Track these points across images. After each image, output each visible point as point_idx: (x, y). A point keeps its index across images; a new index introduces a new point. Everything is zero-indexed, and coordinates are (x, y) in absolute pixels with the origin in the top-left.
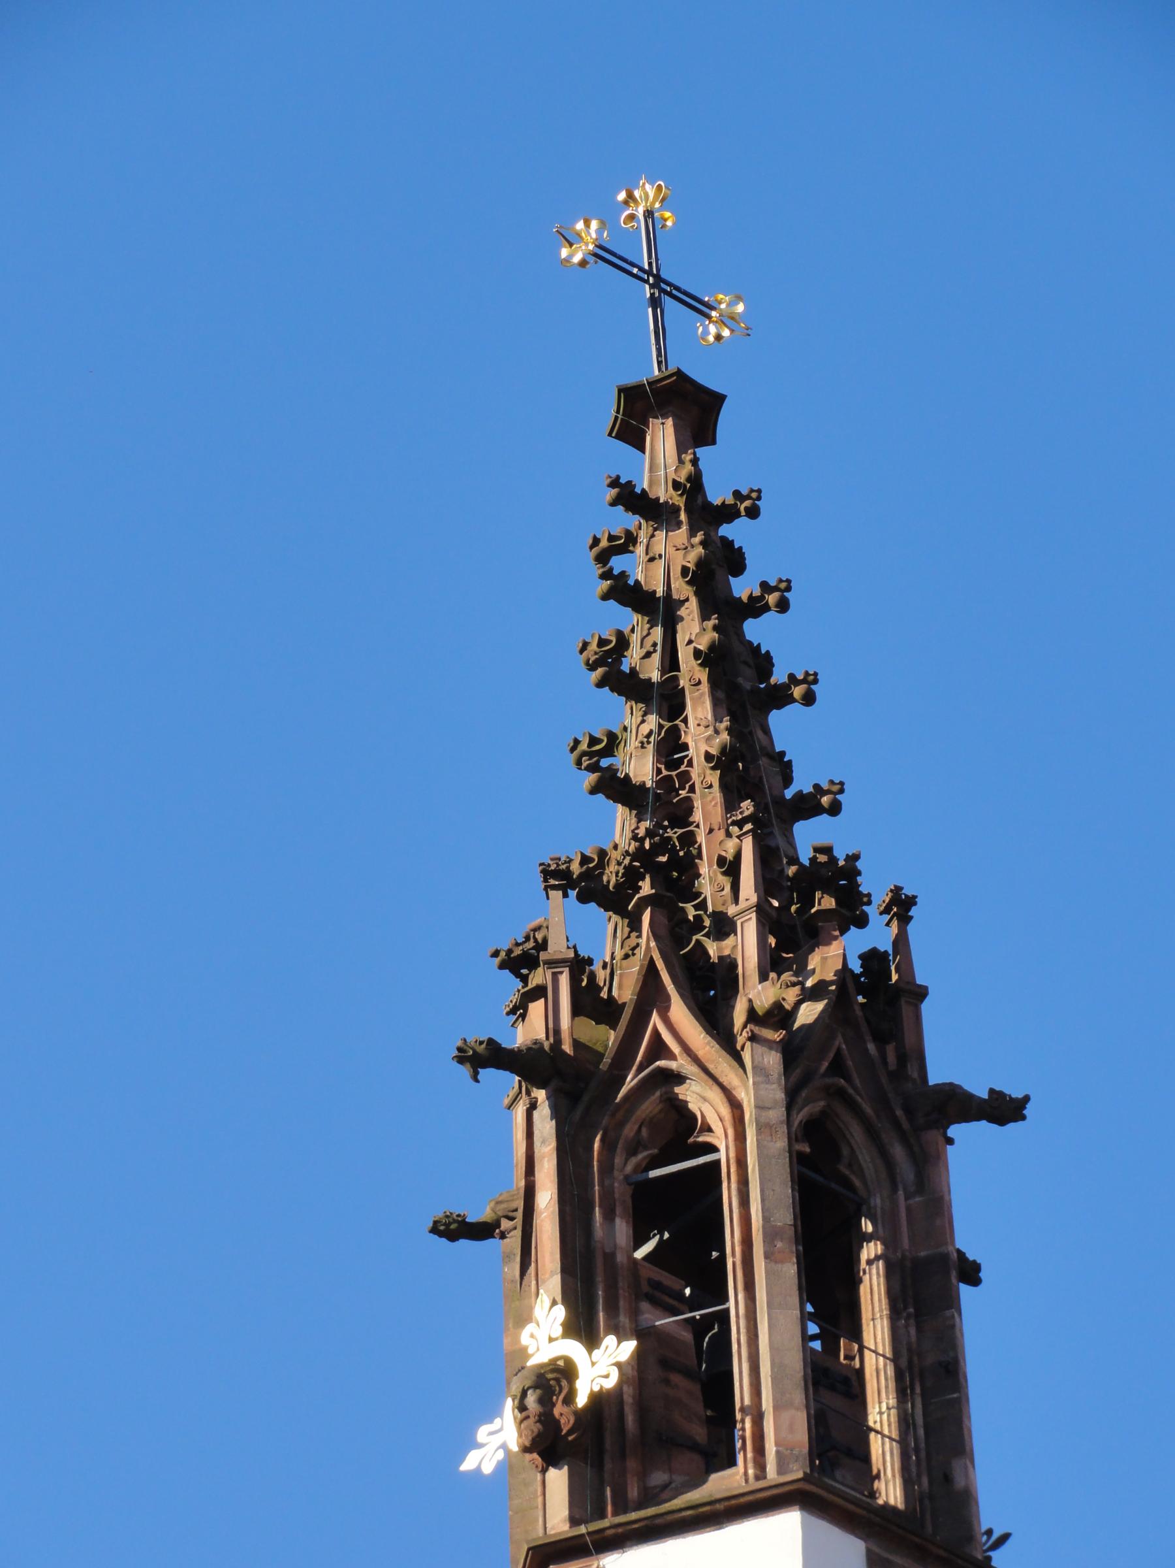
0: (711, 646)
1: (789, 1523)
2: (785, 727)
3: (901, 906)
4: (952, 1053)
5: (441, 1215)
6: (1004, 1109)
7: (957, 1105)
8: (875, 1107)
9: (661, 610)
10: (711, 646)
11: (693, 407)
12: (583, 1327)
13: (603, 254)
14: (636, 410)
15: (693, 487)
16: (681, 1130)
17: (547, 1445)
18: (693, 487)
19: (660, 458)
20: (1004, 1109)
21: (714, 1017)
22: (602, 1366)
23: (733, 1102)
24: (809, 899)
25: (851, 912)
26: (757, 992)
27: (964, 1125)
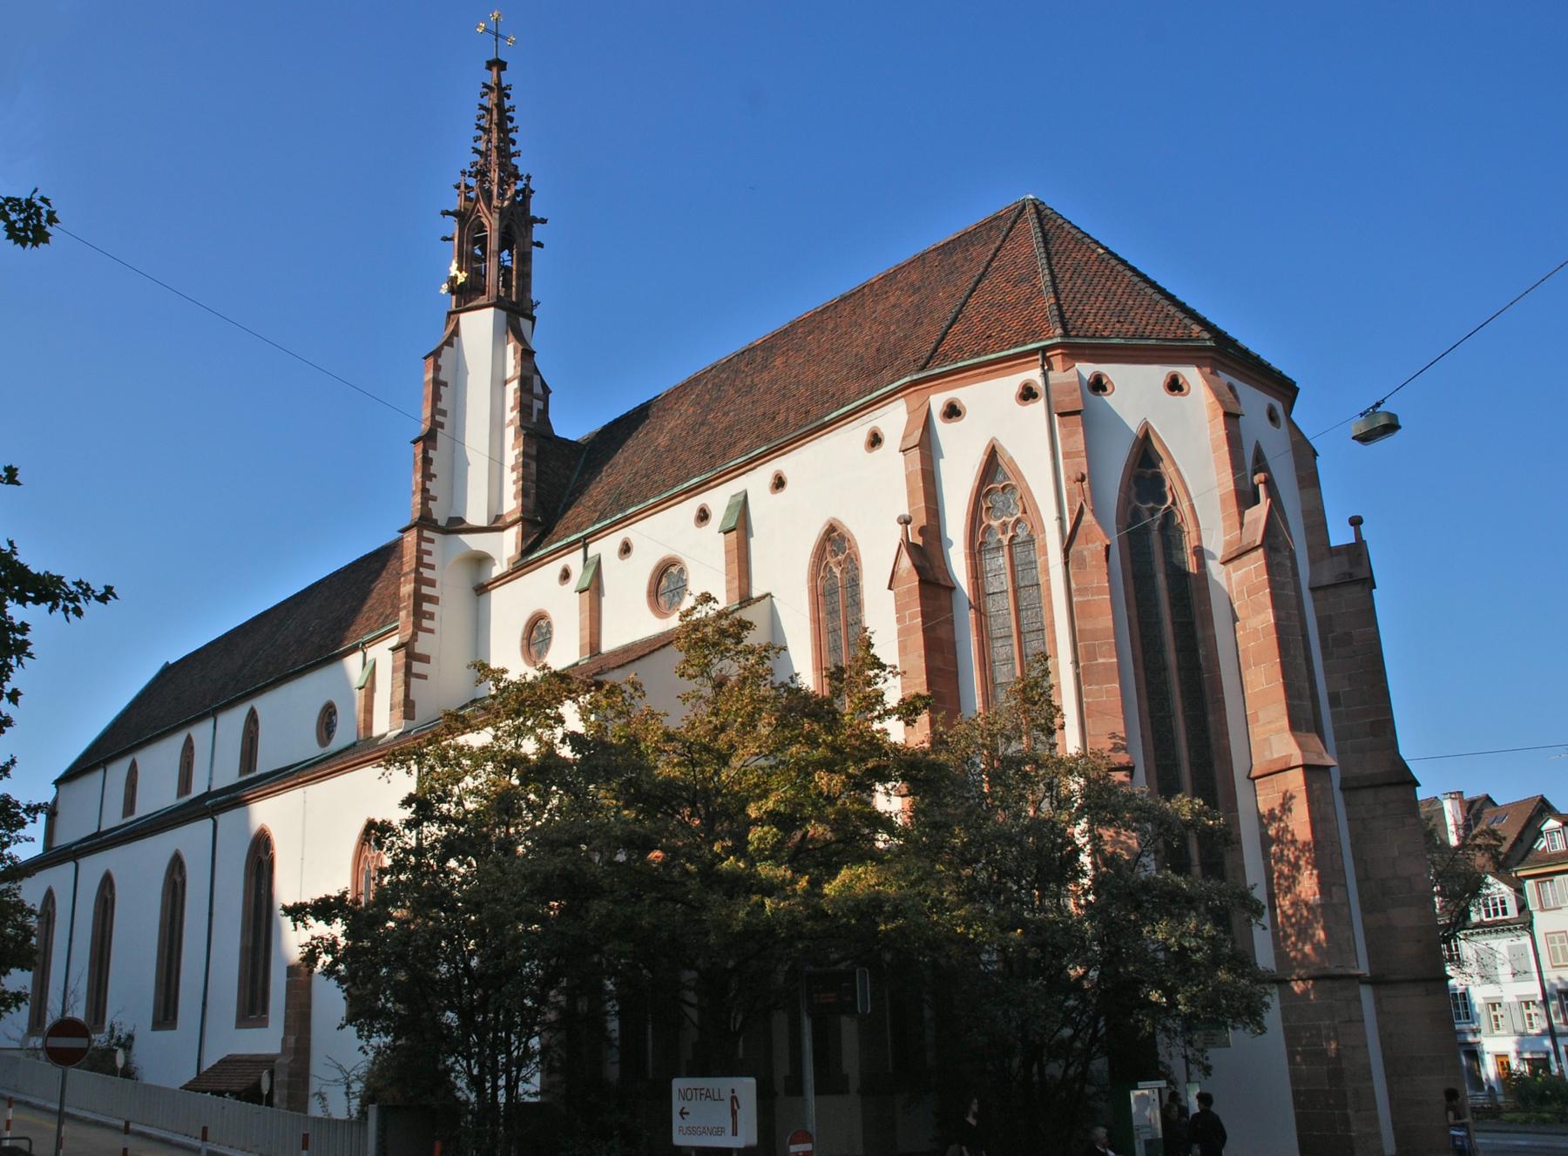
0: (500, 120)
1: (492, 310)
2: (431, 504)
3: (529, 178)
4: (534, 211)
5: (378, 820)
6: (544, 221)
7: (535, 220)
8: (518, 225)
9: (487, 131)
10: (500, 120)
11: (500, 65)
12: (460, 269)
13: (486, 30)
14: (490, 65)
15: (499, 84)
16: (481, 227)
17: (452, 291)
18: (499, 84)
19: (491, 77)
20: (544, 221)
21: (489, 205)
22: (462, 277)
23: (492, 224)
24: (510, 173)
25: (518, 177)
26: (495, 202)
27: (283, 1015)
